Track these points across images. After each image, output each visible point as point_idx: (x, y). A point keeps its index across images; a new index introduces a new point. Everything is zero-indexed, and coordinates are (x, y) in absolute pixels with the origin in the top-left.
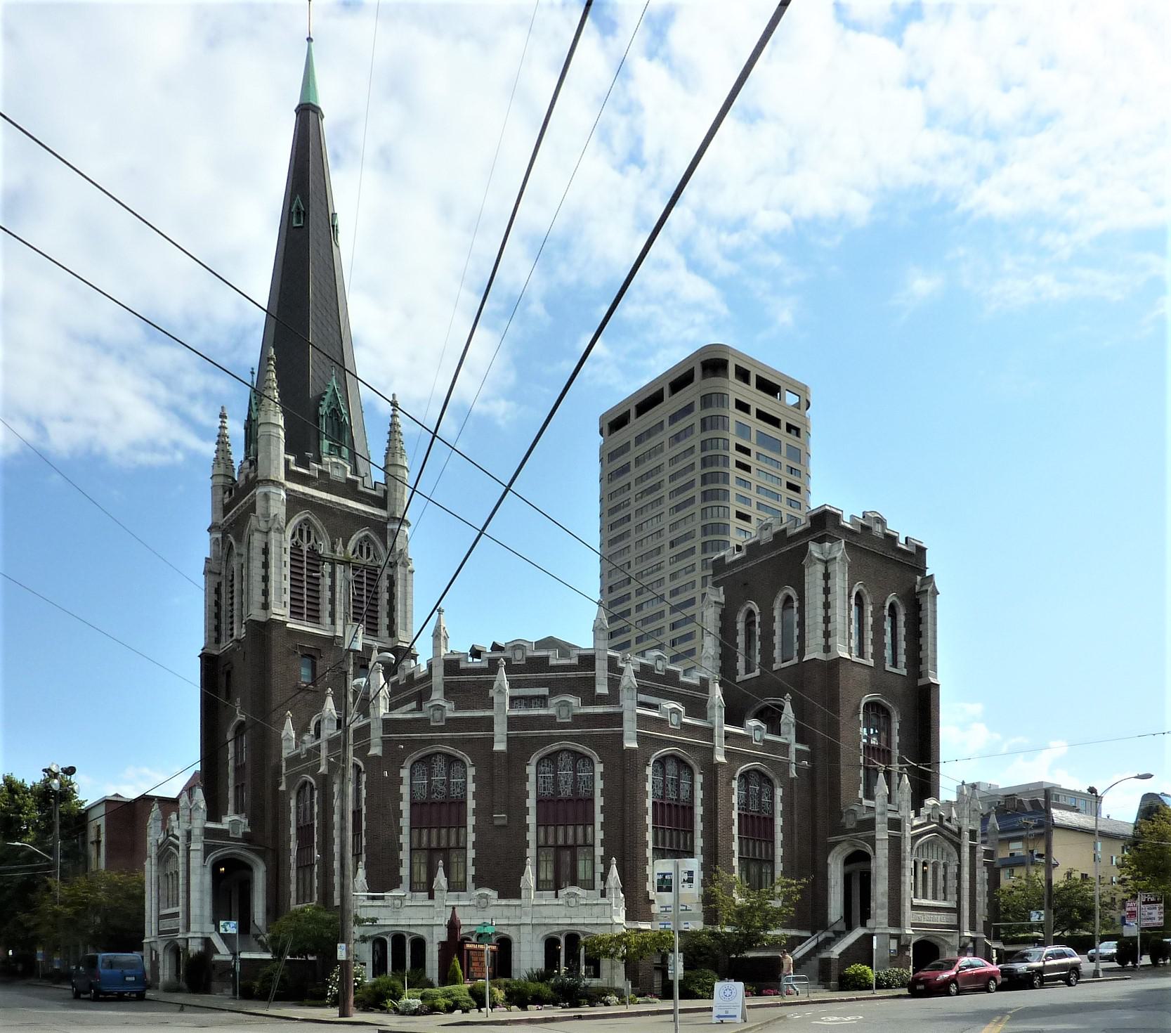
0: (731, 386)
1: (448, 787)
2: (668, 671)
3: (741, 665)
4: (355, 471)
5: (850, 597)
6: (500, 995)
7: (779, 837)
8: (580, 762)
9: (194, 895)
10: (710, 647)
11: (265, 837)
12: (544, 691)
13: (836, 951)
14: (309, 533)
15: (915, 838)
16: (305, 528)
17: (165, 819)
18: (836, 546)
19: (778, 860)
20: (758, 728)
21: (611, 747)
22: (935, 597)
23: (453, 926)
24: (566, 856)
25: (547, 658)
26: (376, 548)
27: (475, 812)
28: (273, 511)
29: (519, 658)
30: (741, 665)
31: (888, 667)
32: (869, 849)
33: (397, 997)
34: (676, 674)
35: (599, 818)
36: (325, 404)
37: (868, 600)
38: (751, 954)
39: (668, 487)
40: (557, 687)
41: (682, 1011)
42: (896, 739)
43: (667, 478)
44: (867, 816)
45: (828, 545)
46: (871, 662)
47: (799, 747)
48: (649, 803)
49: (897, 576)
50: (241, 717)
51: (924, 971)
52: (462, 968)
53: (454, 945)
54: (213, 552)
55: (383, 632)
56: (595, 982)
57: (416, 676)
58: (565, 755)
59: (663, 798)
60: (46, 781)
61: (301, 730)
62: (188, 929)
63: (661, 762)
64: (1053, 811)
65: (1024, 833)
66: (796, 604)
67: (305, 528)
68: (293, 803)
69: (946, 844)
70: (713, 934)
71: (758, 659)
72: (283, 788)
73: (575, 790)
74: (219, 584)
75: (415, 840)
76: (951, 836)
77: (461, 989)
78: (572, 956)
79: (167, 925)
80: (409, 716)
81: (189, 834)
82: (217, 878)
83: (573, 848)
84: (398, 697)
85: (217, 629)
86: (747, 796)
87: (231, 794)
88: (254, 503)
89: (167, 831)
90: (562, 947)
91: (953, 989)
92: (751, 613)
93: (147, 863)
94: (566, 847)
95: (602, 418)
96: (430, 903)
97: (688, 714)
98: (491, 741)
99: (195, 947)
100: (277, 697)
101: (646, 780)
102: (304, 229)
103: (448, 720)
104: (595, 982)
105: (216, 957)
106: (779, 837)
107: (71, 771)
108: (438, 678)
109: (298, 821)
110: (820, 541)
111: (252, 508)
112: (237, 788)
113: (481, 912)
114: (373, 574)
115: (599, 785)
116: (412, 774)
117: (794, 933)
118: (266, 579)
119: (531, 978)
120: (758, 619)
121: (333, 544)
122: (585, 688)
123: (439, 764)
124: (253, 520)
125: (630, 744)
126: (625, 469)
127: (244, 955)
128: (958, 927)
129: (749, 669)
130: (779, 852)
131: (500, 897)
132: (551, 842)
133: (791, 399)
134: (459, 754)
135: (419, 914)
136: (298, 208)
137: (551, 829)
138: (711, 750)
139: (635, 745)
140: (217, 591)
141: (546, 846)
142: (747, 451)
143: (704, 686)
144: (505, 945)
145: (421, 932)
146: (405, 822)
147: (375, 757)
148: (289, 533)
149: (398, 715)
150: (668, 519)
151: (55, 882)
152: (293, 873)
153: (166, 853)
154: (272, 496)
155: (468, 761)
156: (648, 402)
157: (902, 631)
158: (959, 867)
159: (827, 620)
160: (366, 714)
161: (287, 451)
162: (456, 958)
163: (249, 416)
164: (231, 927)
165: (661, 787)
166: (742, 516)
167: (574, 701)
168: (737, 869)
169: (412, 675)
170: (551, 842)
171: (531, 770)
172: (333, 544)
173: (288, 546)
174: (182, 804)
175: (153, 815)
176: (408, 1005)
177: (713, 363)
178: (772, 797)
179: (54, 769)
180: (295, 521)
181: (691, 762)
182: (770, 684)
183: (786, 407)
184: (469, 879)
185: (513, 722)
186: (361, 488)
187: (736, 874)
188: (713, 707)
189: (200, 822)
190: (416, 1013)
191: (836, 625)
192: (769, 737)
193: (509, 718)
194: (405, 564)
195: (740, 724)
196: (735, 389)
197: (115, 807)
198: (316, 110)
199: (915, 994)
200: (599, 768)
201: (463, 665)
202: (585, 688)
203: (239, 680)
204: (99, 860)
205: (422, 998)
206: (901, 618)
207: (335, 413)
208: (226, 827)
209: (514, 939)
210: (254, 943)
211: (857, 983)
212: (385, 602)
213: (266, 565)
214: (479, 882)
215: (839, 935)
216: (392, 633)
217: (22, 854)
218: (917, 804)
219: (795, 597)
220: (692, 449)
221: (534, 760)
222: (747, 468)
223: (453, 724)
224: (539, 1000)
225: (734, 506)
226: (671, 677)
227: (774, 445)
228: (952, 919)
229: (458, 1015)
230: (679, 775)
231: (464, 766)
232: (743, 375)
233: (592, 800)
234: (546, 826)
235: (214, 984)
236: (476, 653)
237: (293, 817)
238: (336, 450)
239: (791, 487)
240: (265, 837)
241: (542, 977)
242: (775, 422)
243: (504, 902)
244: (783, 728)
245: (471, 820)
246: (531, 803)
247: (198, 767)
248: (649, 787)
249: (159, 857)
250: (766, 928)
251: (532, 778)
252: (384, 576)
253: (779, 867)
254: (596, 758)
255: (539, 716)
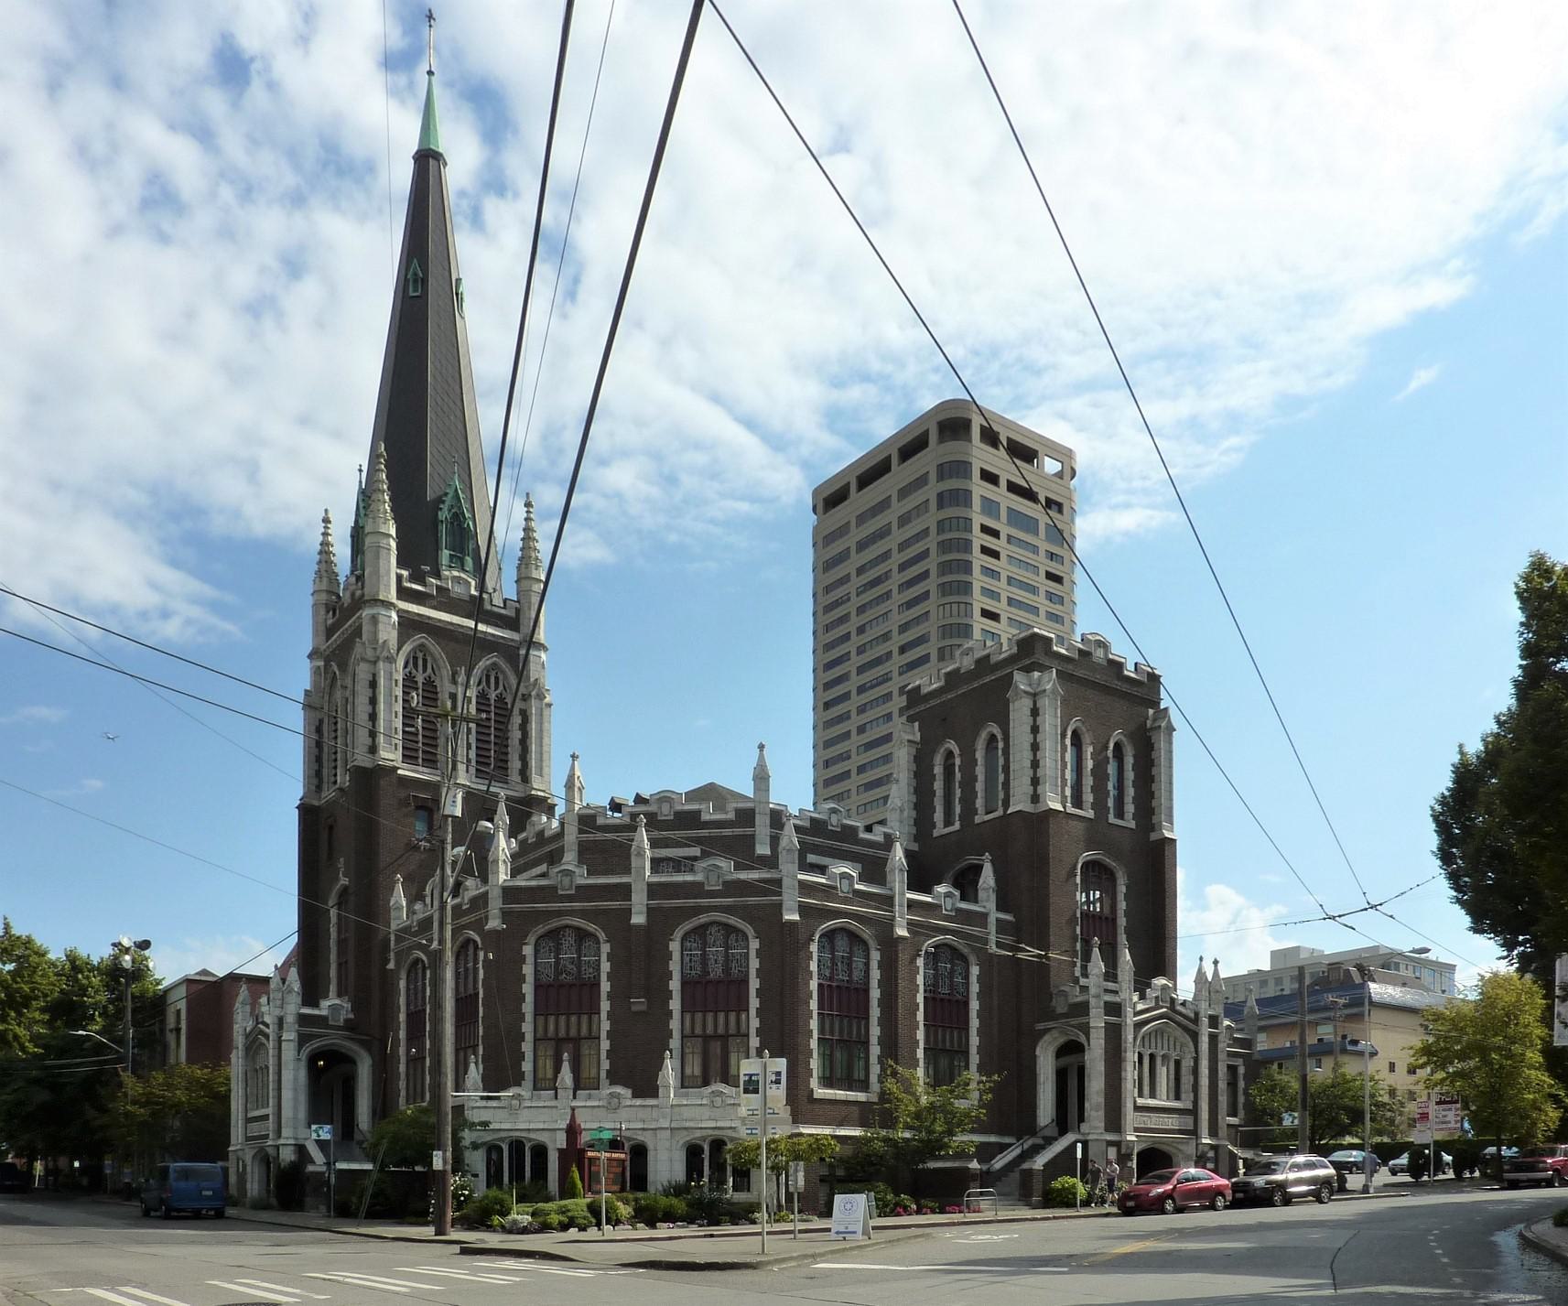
0: (975, 452)
1: (579, 968)
2: (844, 827)
3: (939, 816)
4: (482, 587)
5: (1063, 736)
6: (625, 1210)
7: (974, 1023)
8: (733, 937)
9: (287, 1094)
10: (900, 793)
11: (370, 1023)
12: (696, 851)
13: (1039, 1162)
14: (425, 661)
15: (1139, 1025)
16: (420, 655)
17: (254, 1003)
18: (1046, 676)
19: (973, 1050)
20: (948, 895)
21: (768, 920)
22: (1170, 735)
23: (573, 1131)
24: (716, 1047)
25: (699, 812)
26: (506, 678)
27: (610, 996)
28: (382, 637)
29: (666, 813)
30: (939, 816)
31: (1112, 819)
32: (1083, 1039)
33: (504, 1213)
34: (854, 830)
35: (754, 1003)
36: (445, 507)
37: (1087, 739)
38: (932, 1165)
39: (897, 579)
40: (713, 846)
41: (801, 1231)
42: (1122, 905)
43: (895, 568)
44: (1079, 999)
45: (1036, 674)
46: (1090, 814)
47: (1002, 916)
48: (814, 985)
49: (1125, 710)
50: (344, 881)
51: (1145, 1182)
52: (582, 1179)
53: (574, 1154)
54: (315, 684)
55: (515, 777)
56: (741, 1197)
57: (547, 834)
58: (714, 929)
59: (831, 979)
60: (116, 957)
61: (416, 896)
62: (279, 1134)
63: (829, 936)
64: (1372, 985)
65: (1331, 1014)
66: (1001, 745)
67: (420, 655)
68: (402, 984)
69: (1179, 1032)
70: (886, 1140)
71: (958, 810)
72: (391, 966)
73: (727, 970)
74: (321, 721)
75: (540, 1029)
76: (1186, 1022)
77: (579, 1204)
78: (718, 1167)
79: (255, 1129)
80: (533, 883)
81: (281, 1021)
82: (314, 1074)
83: (725, 1038)
84: (553, 846)
85: (318, 774)
86: (935, 976)
87: (333, 973)
88: (360, 627)
89: (258, 1019)
90: (706, 1155)
91: (1169, 1205)
92: (950, 754)
93: (233, 1057)
94: (716, 1037)
95: (816, 493)
96: (553, 1103)
97: (862, 879)
98: (628, 912)
99: (287, 1155)
100: (384, 858)
101: (810, 958)
102: (423, 297)
103: (579, 887)
104: (741, 1197)
105: (310, 1168)
106: (974, 1023)
107: (145, 945)
108: (571, 837)
109: (408, 1005)
110: (1028, 670)
111: (358, 632)
112: (339, 965)
113: (607, 1114)
114: (504, 713)
115: (754, 964)
116: (536, 952)
117: (993, 1139)
118: (373, 717)
119: (666, 1193)
120: (958, 761)
121: (454, 674)
122: (741, 849)
123: (569, 940)
124: (358, 649)
125: (792, 916)
126: (842, 557)
127: (341, 1166)
128: (1194, 1132)
129: (948, 823)
130: (974, 1040)
131: (635, 1096)
132: (698, 1031)
133: (1051, 466)
134: (592, 927)
135: (533, 1115)
136: (415, 274)
137: (699, 1016)
138: (890, 924)
139: (796, 917)
140: (319, 730)
141: (693, 1035)
142: (995, 534)
143: (889, 842)
144: (639, 1152)
145: (641, 1137)
146: (528, 1007)
147: (495, 932)
148: (401, 662)
149: (521, 882)
150: (897, 619)
151: (127, 1078)
152: (402, 1068)
153: (254, 1044)
154: (381, 618)
155: (602, 936)
156: (872, 471)
157: (1130, 775)
158: (1196, 1060)
159: (1035, 764)
160: (485, 880)
161: (400, 564)
162: (574, 1169)
163: (356, 522)
164: (325, 1133)
165: (829, 967)
166: (987, 614)
167: (726, 865)
168: (921, 1063)
169: (542, 832)
170: (698, 1031)
171: (675, 947)
172: (454, 674)
173: (400, 677)
174: (272, 986)
175: (240, 998)
176: (515, 1222)
177: (953, 423)
178: (967, 977)
179: (126, 942)
180: (407, 648)
181: (865, 936)
182: (973, 839)
183: (1046, 477)
184: (603, 1074)
185: (653, 890)
186: (488, 607)
187: (920, 1072)
188: (893, 871)
189: (293, 1007)
190: (525, 1231)
191: (1046, 770)
192: (964, 905)
193: (649, 885)
194: (541, 697)
195: (927, 890)
196: (982, 456)
197: (195, 987)
198: (437, 156)
199: (1127, 1212)
200: (754, 945)
201: (600, 821)
202: (741, 849)
203: (344, 838)
204: (180, 1052)
205: (533, 1215)
206: (1129, 761)
207: (458, 518)
208: (324, 1013)
209: (650, 1146)
210: (357, 1151)
211: (1064, 1200)
212: (516, 742)
213: (373, 701)
214: (614, 1078)
215: (1049, 1141)
216: (525, 778)
217: (87, 1045)
218: (1141, 986)
219: (999, 737)
220: (926, 532)
221: (678, 934)
222: (996, 555)
223: (585, 892)
224: (670, 1217)
225: (979, 602)
226: (848, 833)
227: (1030, 525)
228: (1188, 1122)
229: (573, 1233)
230: (851, 952)
231: (598, 942)
232: (990, 437)
233: (745, 982)
234: (693, 1013)
235: (309, 1200)
236: (616, 806)
237: (402, 1000)
238: (457, 561)
239: (1051, 577)
240: (370, 1023)
241: (677, 1190)
242: (1029, 494)
243: (639, 1102)
244: (981, 895)
245: (605, 1006)
246: (675, 985)
247: (295, 938)
248: (814, 966)
249: (248, 1049)
250: (951, 1133)
251: (676, 956)
252: (516, 711)
253: (974, 1059)
254: (750, 931)
255: (685, 883)
